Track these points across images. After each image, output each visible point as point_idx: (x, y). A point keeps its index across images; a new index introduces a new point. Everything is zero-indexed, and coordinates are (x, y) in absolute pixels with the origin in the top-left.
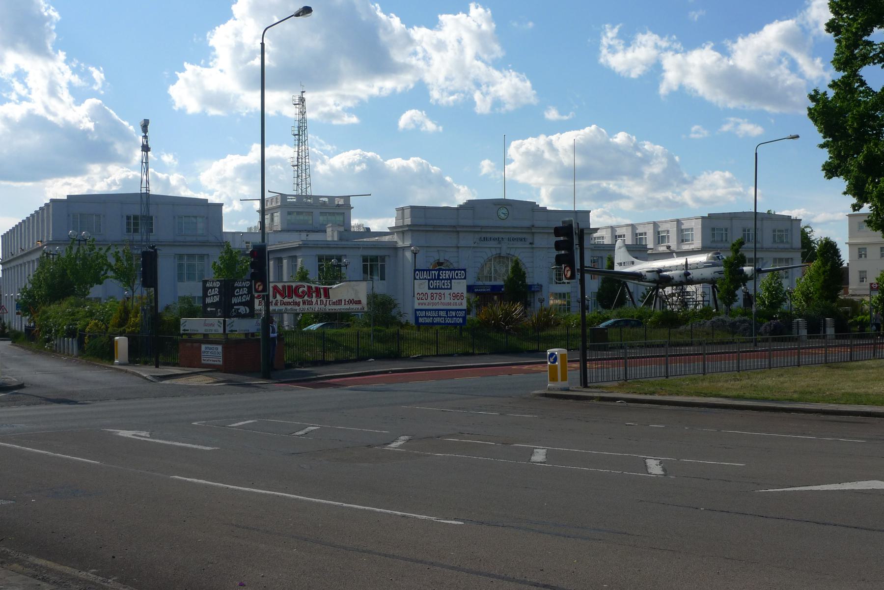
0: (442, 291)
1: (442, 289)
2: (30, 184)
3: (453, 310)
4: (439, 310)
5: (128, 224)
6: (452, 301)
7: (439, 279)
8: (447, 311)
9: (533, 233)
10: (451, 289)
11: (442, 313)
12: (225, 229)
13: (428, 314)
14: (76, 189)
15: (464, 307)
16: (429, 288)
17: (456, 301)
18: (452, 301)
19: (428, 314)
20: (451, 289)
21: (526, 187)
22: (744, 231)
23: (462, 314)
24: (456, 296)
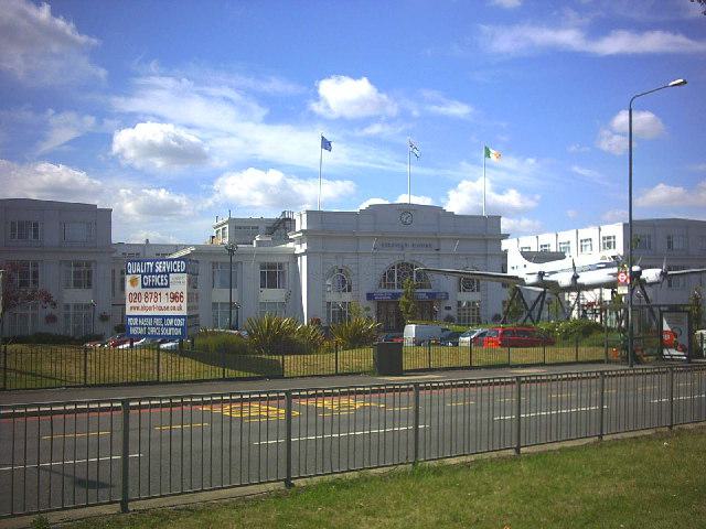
0: (158, 290)
1: (158, 287)
2: (403, 199)
3: (170, 317)
4: (153, 317)
5: (13, 230)
6: (170, 304)
7: (154, 273)
8: (164, 318)
9: (439, 239)
10: (168, 286)
11: (157, 321)
12: (115, 239)
13: (142, 322)
14: (44, 194)
15: (184, 312)
16: (143, 286)
17: (174, 304)
18: (170, 304)
19: (142, 322)
20: (168, 286)
21: (83, 192)
22: (669, 238)
23: (180, 322)
24: (175, 297)
